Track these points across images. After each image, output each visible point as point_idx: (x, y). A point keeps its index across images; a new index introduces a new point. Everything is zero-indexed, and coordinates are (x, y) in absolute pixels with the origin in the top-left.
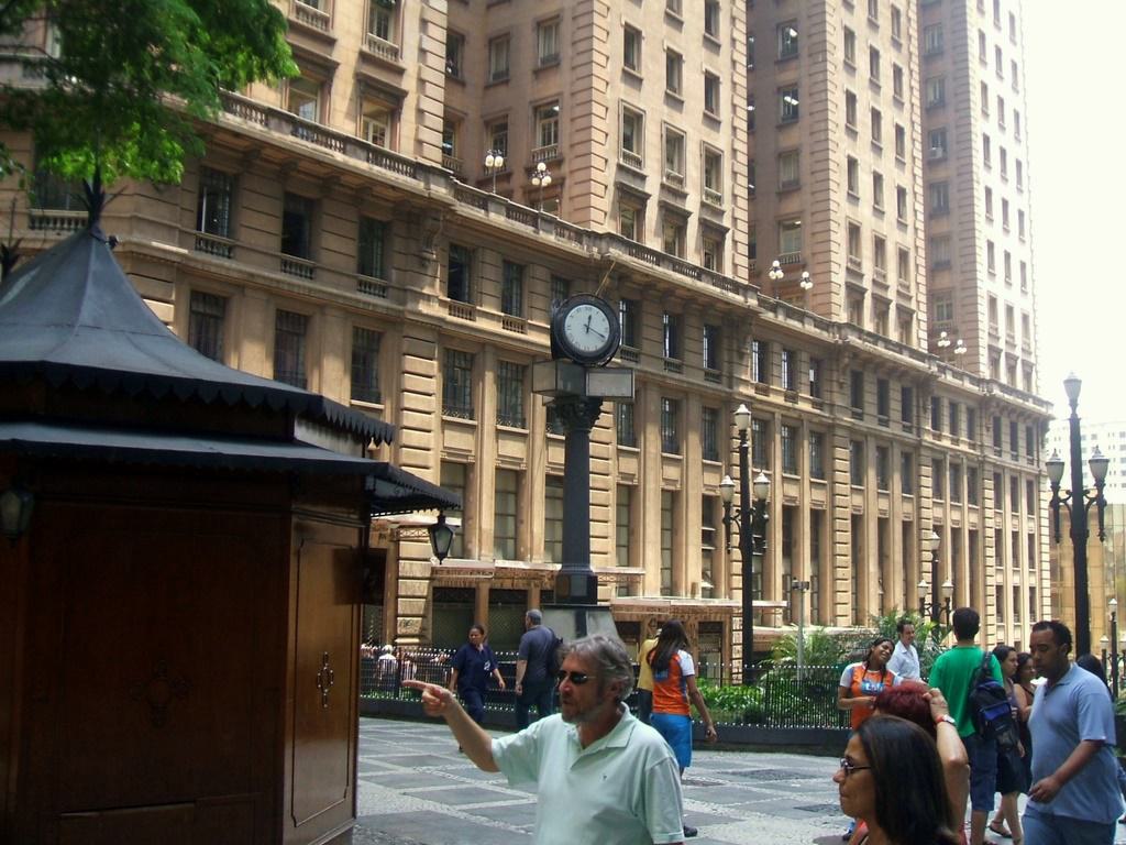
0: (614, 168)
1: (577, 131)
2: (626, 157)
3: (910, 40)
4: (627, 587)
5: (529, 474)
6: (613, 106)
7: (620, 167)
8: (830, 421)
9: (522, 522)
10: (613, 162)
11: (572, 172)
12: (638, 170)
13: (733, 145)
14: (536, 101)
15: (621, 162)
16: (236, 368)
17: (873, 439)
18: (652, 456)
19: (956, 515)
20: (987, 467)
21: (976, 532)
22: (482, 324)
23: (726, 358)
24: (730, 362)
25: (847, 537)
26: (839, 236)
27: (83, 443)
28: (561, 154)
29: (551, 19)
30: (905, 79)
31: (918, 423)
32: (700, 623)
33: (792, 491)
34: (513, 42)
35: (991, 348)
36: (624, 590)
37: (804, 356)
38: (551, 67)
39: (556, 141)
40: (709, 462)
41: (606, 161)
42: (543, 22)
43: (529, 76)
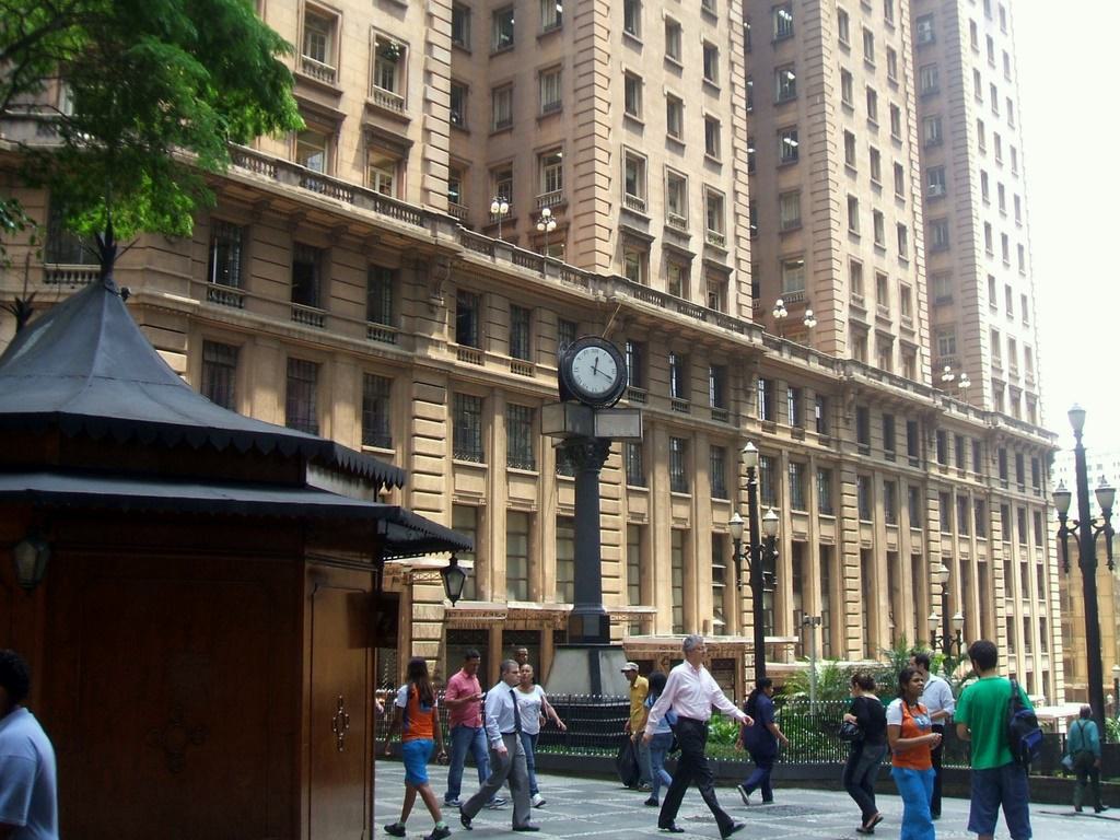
5: (539, 516)
6: (615, 152)
7: (623, 211)
11: (576, 217)
18: (662, 495)
19: (964, 548)
20: (994, 499)
22: (490, 368)
26: (841, 274)
30: (902, 118)
33: (801, 527)
37: (810, 394)
39: (560, 184)
43: (532, 124)
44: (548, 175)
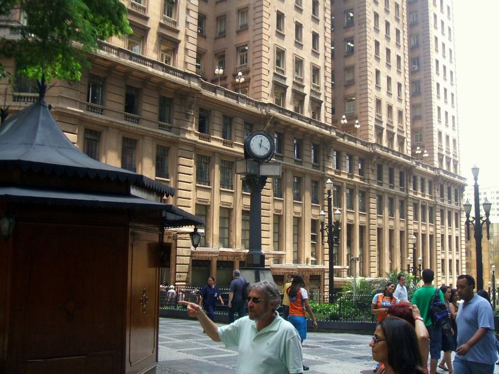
0: (272, 74)
1: (256, 58)
2: (277, 69)
3: (403, 18)
4: (278, 260)
5: (234, 210)
6: (272, 47)
7: (275, 74)
8: (368, 186)
9: (231, 231)
10: (272, 71)
11: (253, 76)
12: (283, 75)
13: (325, 64)
14: (238, 45)
15: (275, 72)
16: (105, 163)
17: (387, 194)
18: (289, 202)
19: (424, 228)
21: (433, 235)
22: (213, 143)
23: (322, 158)
24: (324, 160)
25: (375, 238)
26: (372, 105)
27: (37, 196)
28: (249, 68)
29: (244, 8)
30: (401, 35)
31: (407, 187)
32: (310, 276)
33: (351, 217)
34: (227, 18)
35: (439, 154)
36: (277, 261)
38: (244, 30)
39: (246, 63)
40: (314, 204)
41: (269, 71)
42: (241, 10)
43: (234, 34)
44: (241, 57)
